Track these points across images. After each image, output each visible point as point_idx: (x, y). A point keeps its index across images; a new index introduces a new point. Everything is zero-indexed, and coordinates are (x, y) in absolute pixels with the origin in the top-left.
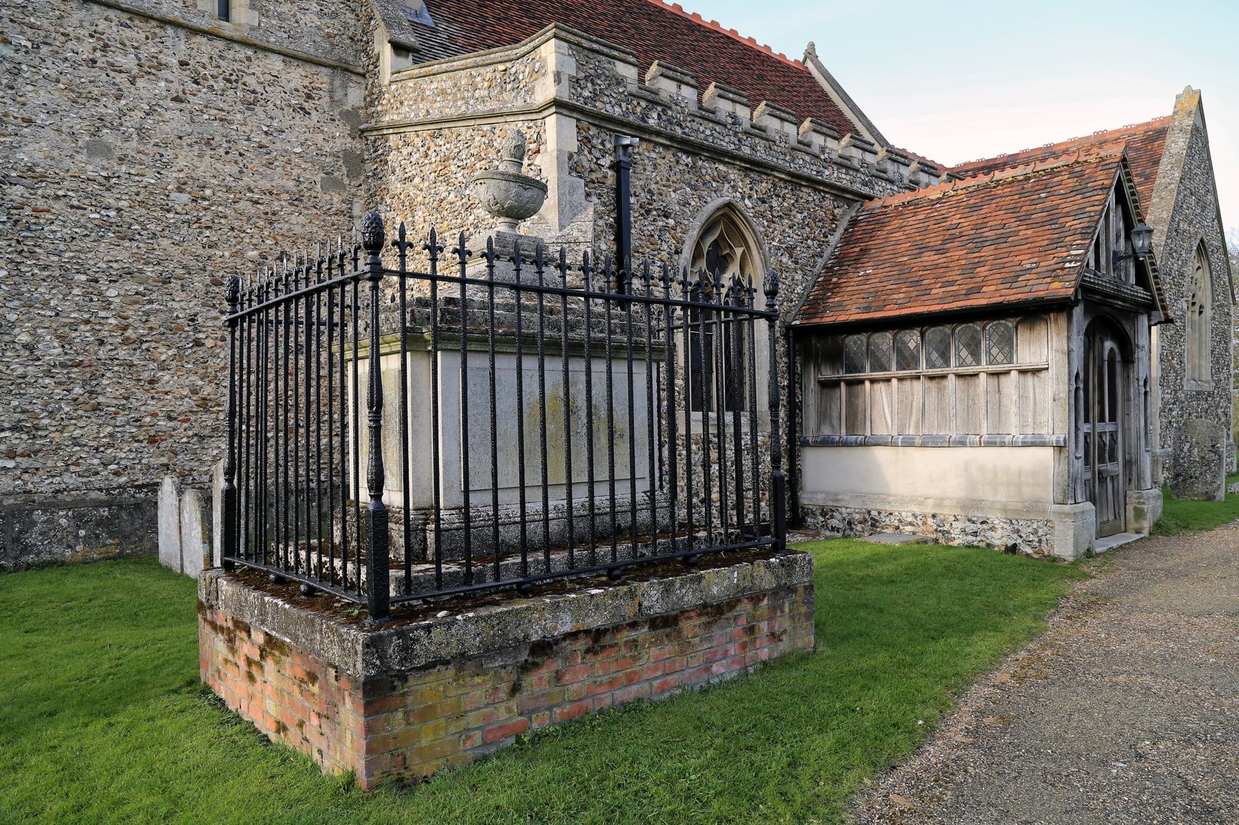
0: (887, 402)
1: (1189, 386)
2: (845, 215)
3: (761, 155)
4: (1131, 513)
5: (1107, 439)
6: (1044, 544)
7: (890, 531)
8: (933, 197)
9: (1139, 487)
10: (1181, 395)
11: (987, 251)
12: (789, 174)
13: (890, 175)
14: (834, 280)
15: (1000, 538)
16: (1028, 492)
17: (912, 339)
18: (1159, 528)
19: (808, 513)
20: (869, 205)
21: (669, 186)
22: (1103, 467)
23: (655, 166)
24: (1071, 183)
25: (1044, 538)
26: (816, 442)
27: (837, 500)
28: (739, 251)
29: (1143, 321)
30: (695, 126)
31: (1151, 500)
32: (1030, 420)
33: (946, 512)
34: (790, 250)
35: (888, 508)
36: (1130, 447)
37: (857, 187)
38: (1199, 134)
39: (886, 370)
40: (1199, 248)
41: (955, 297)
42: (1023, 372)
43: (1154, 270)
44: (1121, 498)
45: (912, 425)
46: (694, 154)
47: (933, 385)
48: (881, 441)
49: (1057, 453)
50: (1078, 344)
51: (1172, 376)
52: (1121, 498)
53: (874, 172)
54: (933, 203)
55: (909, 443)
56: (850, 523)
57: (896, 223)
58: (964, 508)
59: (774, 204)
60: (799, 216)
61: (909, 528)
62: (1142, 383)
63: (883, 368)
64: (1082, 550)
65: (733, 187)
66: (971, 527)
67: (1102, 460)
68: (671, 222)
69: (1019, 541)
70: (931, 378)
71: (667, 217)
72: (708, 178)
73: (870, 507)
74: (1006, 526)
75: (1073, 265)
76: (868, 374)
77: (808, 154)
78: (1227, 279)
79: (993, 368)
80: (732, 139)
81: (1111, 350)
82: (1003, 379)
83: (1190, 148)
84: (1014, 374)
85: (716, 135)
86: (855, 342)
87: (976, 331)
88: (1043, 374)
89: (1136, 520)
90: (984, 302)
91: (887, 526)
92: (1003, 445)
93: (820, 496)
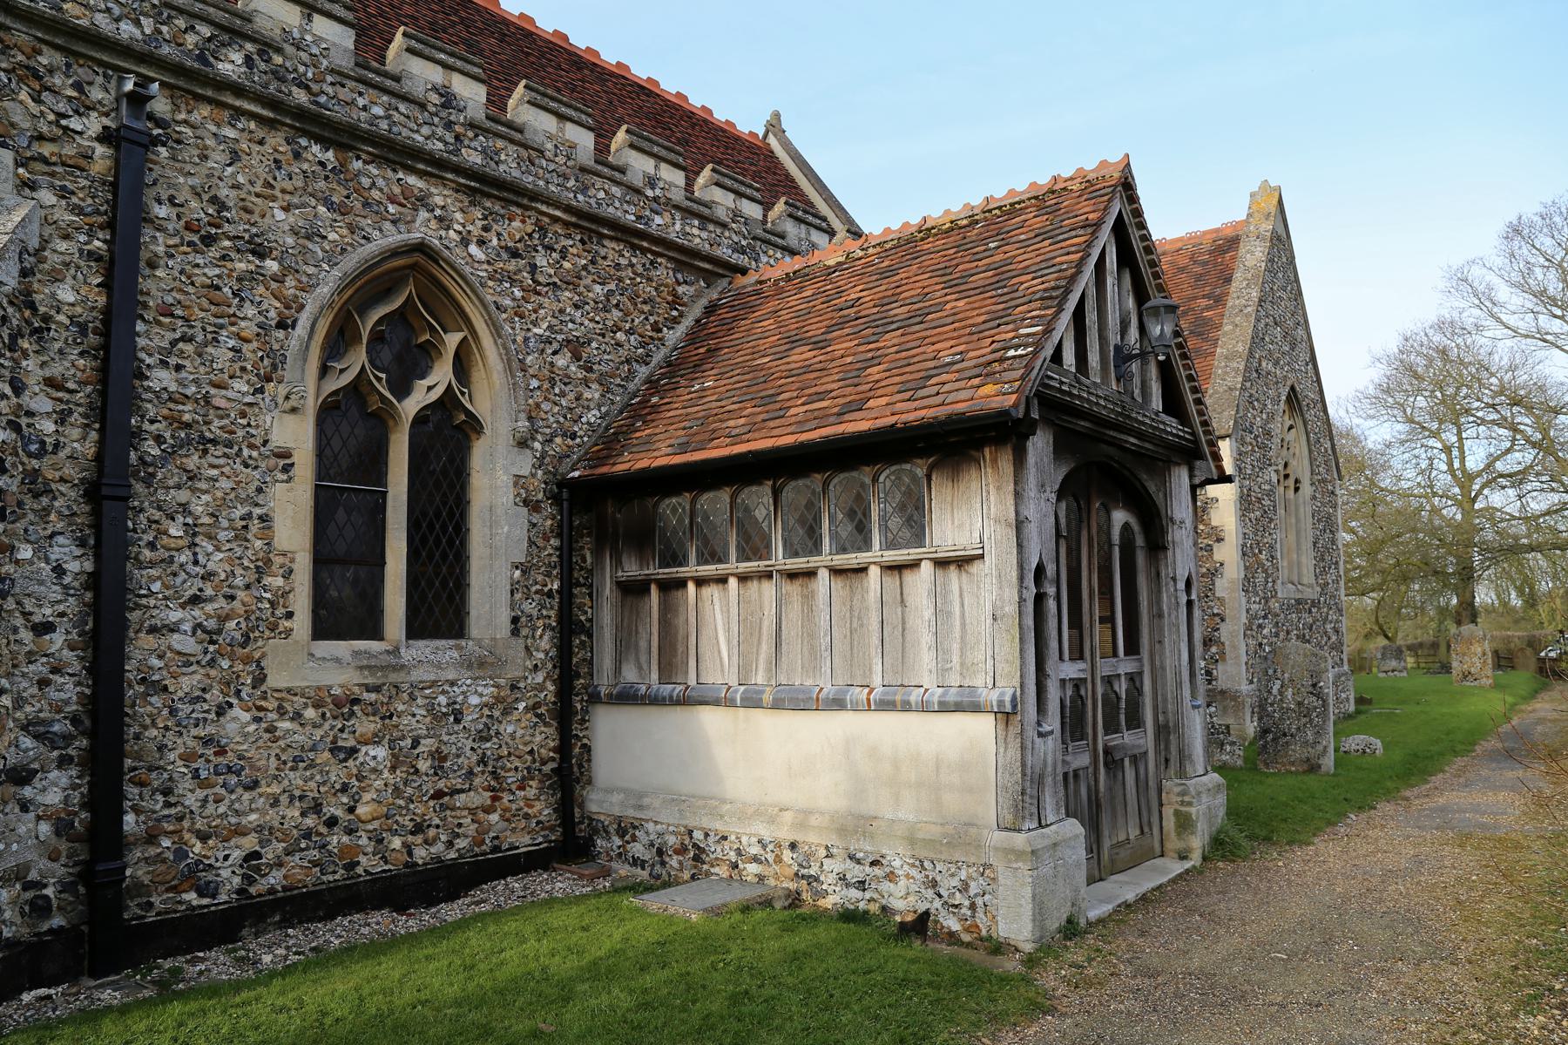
0: (724, 618)
1: (1285, 592)
2: (697, 296)
3: (509, 166)
4: (1170, 823)
5: (1122, 687)
6: (980, 914)
7: (722, 871)
8: (831, 262)
9: (1182, 774)
10: (1275, 605)
11: (892, 339)
12: (568, 209)
13: (792, 241)
14: (655, 400)
15: (903, 898)
16: (953, 803)
17: (759, 499)
18: (1220, 847)
19: (596, 828)
20: (741, 281)
21: (274, 199)
22: (1115, 740)
23: (235, 157)
24: (1039, 222)
25: (979, 901)
26: (610, 696)
27: (640, 807)
28: (452, 340)
29: (1181, 479)
30: (344, 94)
31: (1203, 796)
32: (956, 659)
33: (813, 838)
34: (575, 347)
35: (719, 826)
36: (1165, 700)
37: (723, 252)
38: (1281, 245)
39: (720, 561)
40: (1289, 398)
41: (822, 418)
42: (941, 563)
43: (1195, 390)
44: (1153, 794)
45: (762, 666)
46: (341, 147)
47: (793, 589)
48: (710, 695)
49: (1001, 726)
50: (1042, 509)
51: (1260, 577)
52: (1153, 794)
53: (759, 232)
54: (830, 271)
55: (752, 701)
56: (660, 852)
57: (772, 305)
58: (842, 831)
59: (541, 261)
60: (598, 288)
61: (753, 868)
62: (1181, 585)
63: (716, 557)
64: (1055, 922)
65: (440, 219)
66: (856, 872)
67: (1111, 727)
68: (272, 266)
69: (937, 904)
70: (792, 576)
71: (262, 257)
72: (376, 194)
73: (691, 823)
74: (914, 872)
75: (1020, 352)
76: (692, 569)
77: (618, 183)
78: (1328, 445)
79: (892, 556)
80: (440, 131)
81: (1126, 527)
82: (909, 576)
83: (1271, 261)
84: (927, 567)
85: (396, 117)
86: (674, 510)
87: (863, 485)
88: (976, 568)
89: (1179, 834)
90: (864, 426)
91: (717, 862)
92: (906, 707)
93: (616, 798)
